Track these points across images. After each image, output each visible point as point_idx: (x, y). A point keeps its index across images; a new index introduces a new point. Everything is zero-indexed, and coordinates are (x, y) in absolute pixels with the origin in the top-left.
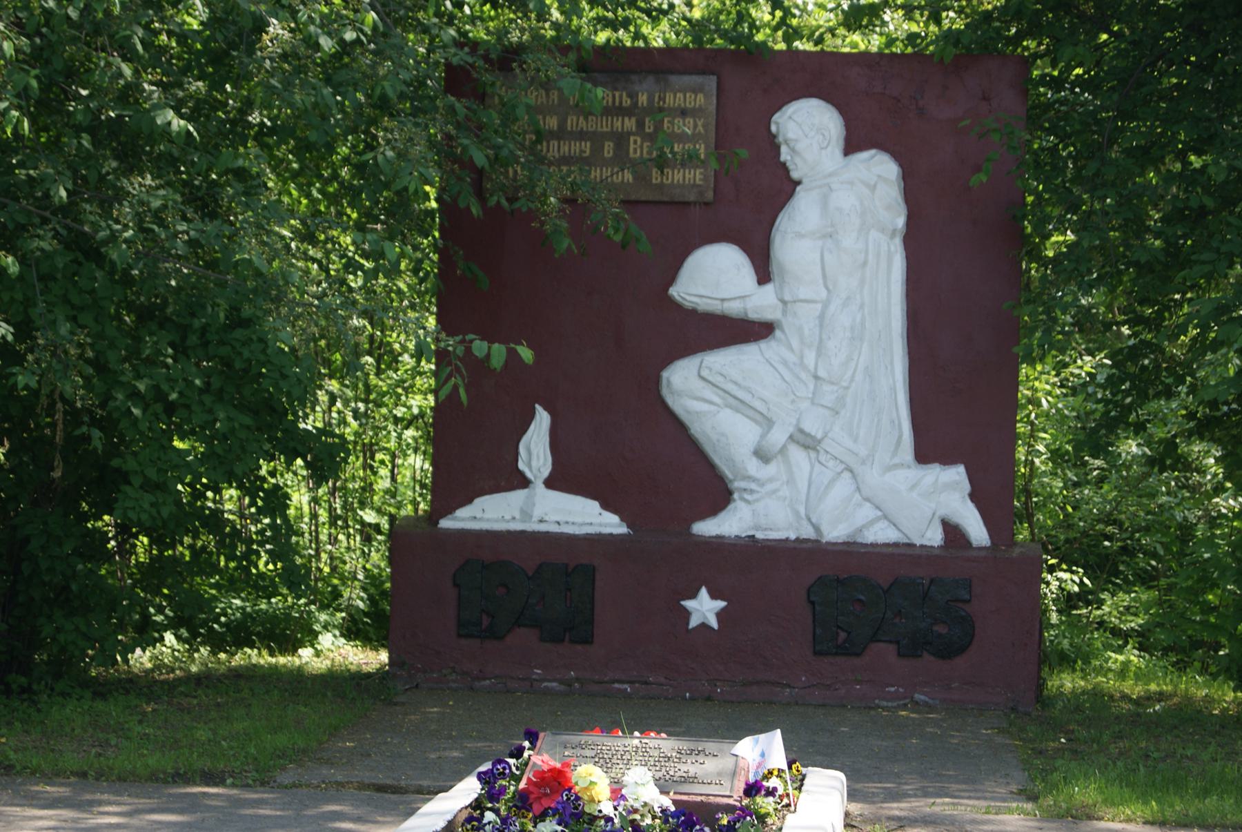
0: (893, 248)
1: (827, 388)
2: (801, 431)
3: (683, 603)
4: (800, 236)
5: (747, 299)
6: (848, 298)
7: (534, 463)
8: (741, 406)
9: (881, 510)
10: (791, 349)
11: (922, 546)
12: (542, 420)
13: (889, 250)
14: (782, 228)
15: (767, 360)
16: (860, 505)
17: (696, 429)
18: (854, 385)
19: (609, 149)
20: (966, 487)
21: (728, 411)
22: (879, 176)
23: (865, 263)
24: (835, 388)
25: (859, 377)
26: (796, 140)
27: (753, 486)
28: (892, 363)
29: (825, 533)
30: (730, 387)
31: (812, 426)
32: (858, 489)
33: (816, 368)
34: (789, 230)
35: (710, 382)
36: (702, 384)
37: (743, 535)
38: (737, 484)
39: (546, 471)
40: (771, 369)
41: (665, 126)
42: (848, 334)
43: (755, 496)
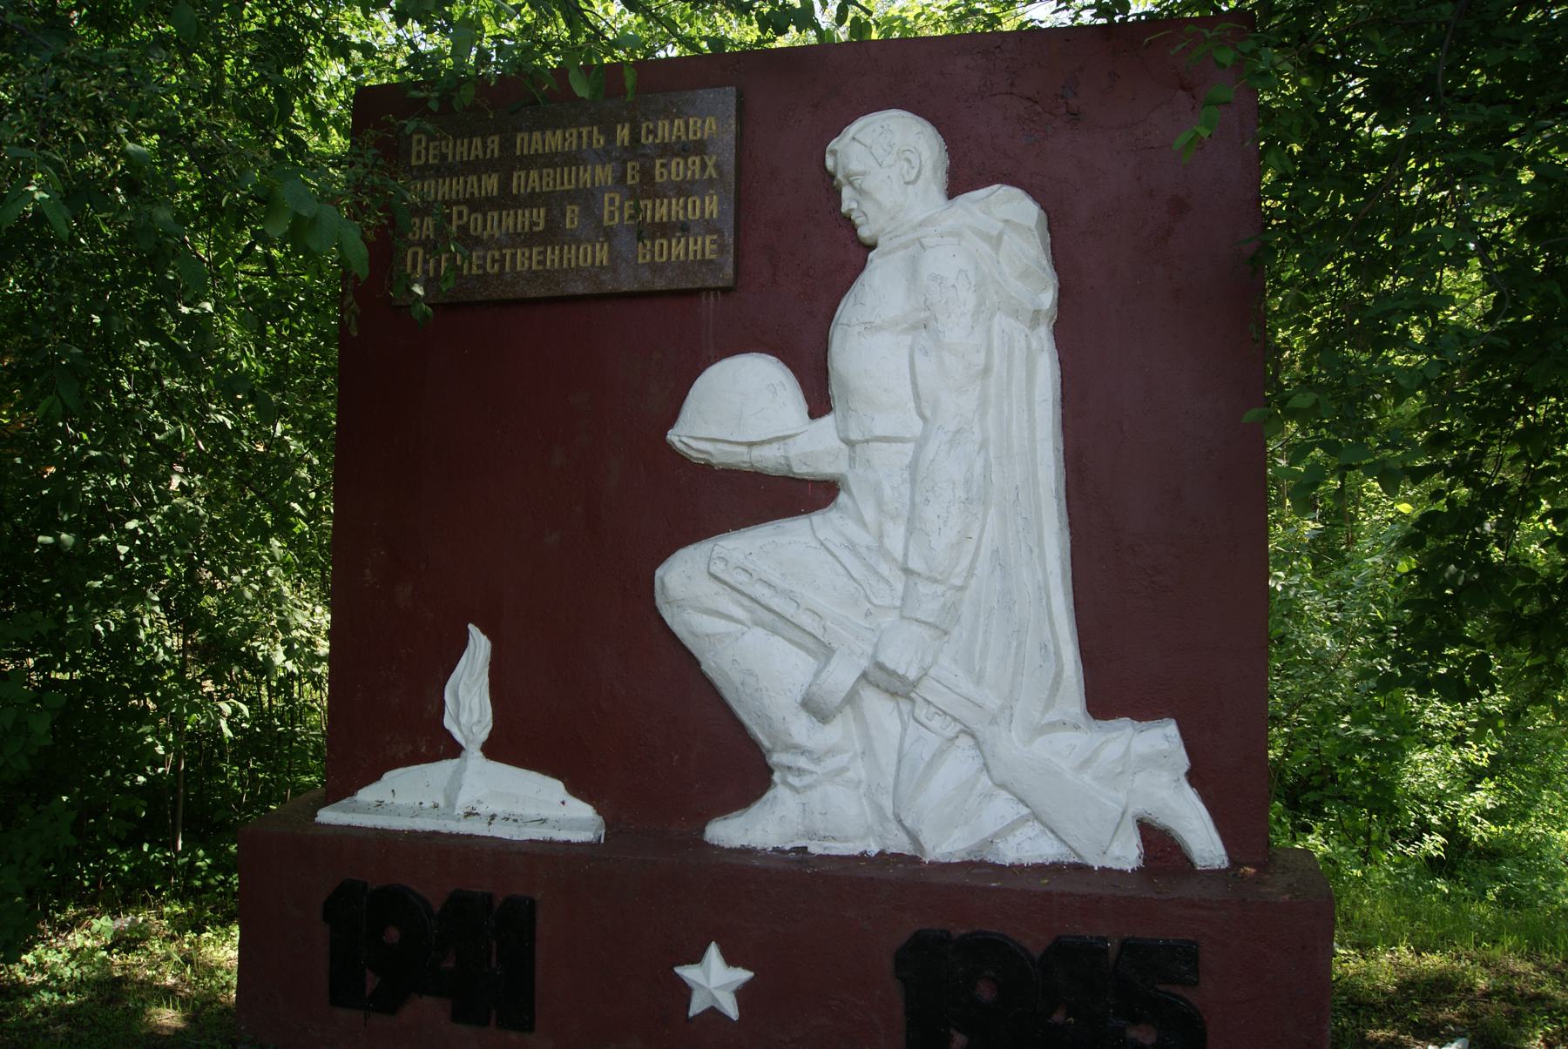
0: (1035, 344)
1: (924, 589)
2: (881, 667)
3: (678, 970)
4: (871, 328)
5: (790, 441)
6: (959, 431)
7: (464, 719)
8: (779, 624)
9: (1027, 806)
10: (862, 523)
11: (1105, 871)
12: (479, 647)
13: (1029, 347)
14: (843, 320)
15: (822, 544)
16: (989, 796)
17: (712, 663)
18: (973, 582)
19: (572, 218)
20: (1182, 761)
21: (759, 631)
22: (1006, 221)
23: (987, 370)
24: (940, 589)
25: (983, 566)
26: (864, 174)
27: (802, 762)
28: (1040, 538)
29: (928, 846)
30: (760, 591)
31: (902, 659)
32: (986, 767)
33: (906, 555)
34: (854, 321)
35: (725, 583)
36: (716, 587)
37: (787, 848)
38: (776, 758)
39: (483, 735)
40: (830, 558)
41: (657, 173)
42: (960, 494)
43: (807, 780)
